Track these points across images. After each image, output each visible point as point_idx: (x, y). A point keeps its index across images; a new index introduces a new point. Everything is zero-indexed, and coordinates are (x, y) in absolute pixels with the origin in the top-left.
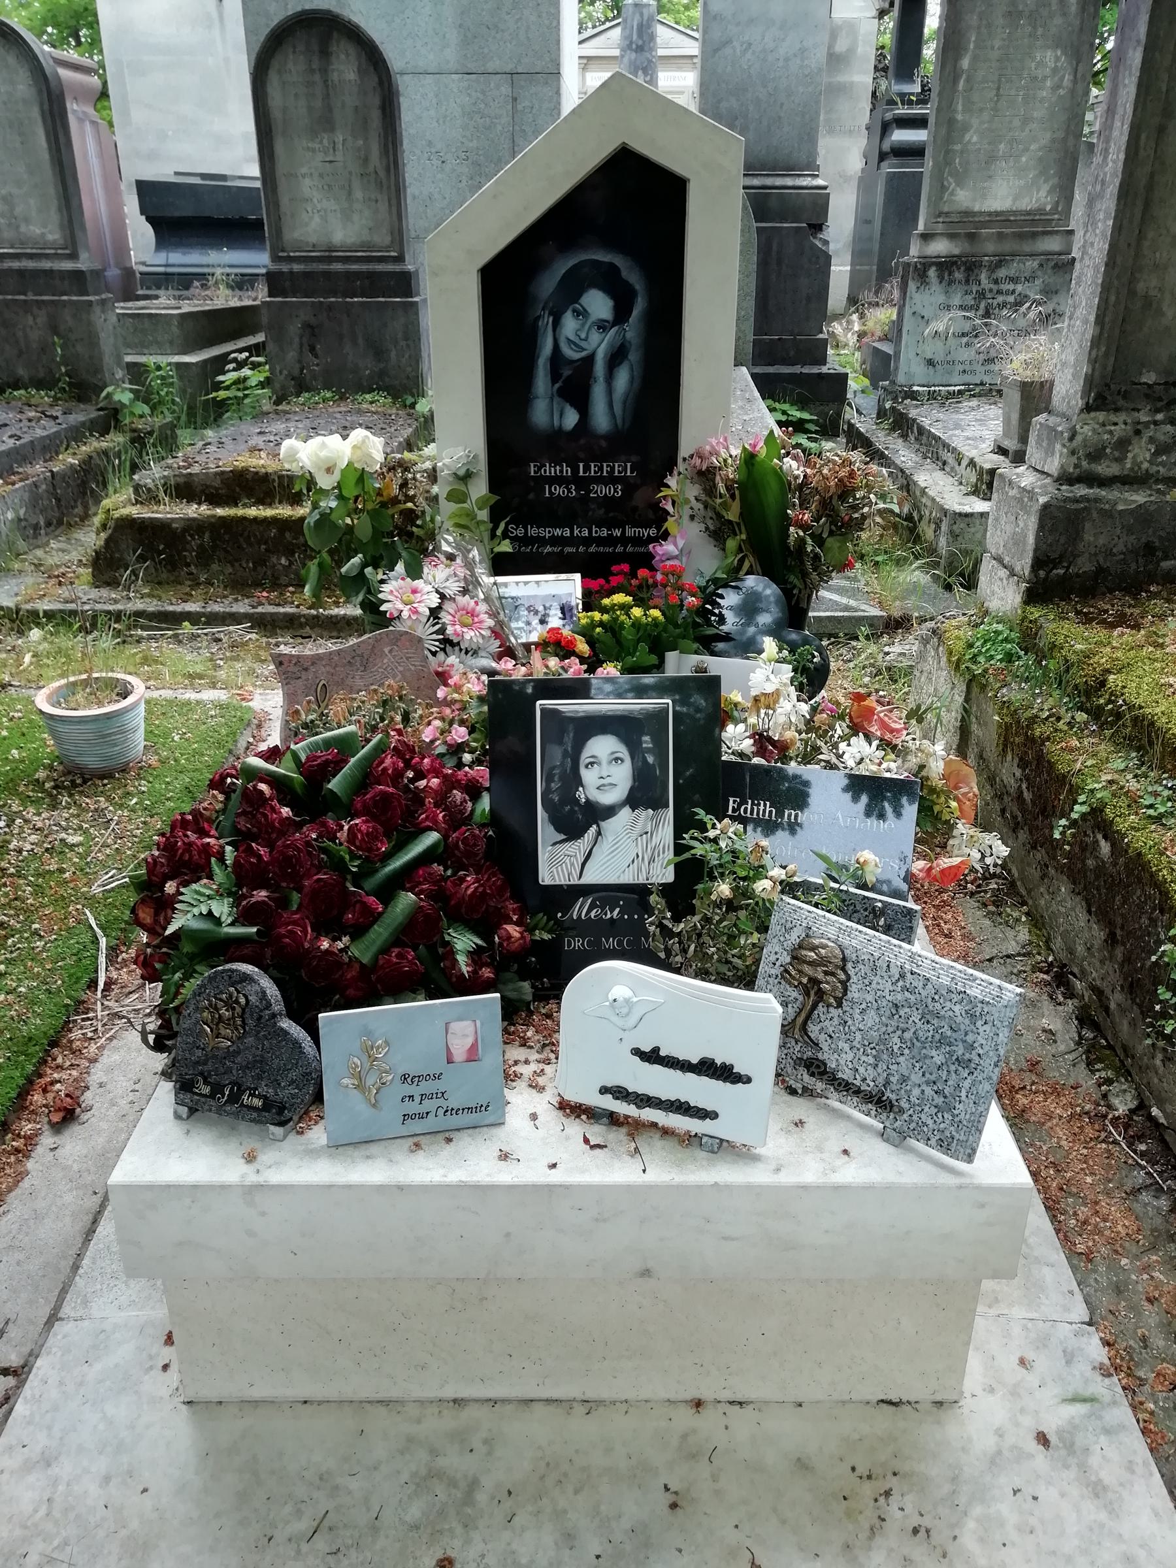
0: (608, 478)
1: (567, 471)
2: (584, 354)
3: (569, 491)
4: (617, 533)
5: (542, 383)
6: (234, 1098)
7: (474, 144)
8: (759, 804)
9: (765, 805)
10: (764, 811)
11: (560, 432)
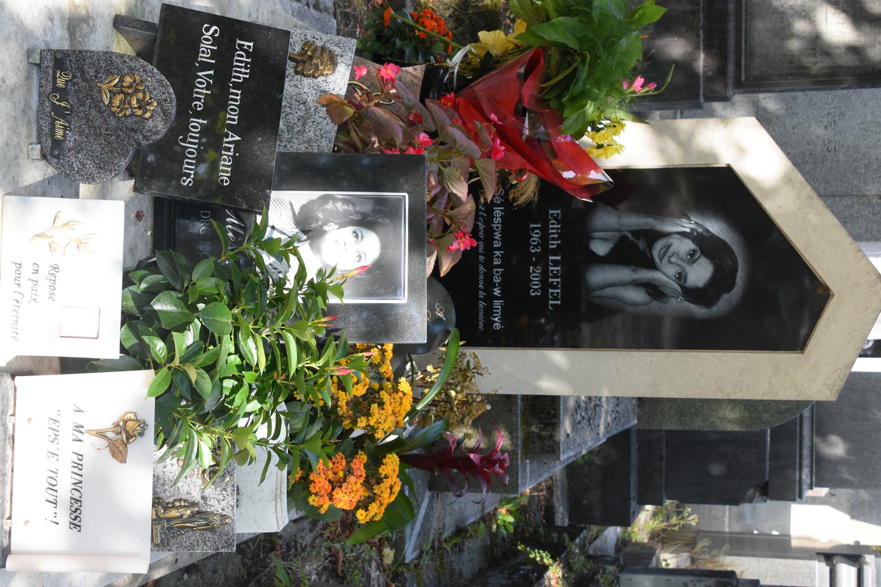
0: (544, 280)
1: (553, 245)
2: (657, 260)
3: (535, 246)
4: (497, 292)
5: (633, 221)
6: (59, 112)
7: (841, 157)
8: (246, 68)
9: (245, 73)
10: (240, 72)
11: (588, 237)
